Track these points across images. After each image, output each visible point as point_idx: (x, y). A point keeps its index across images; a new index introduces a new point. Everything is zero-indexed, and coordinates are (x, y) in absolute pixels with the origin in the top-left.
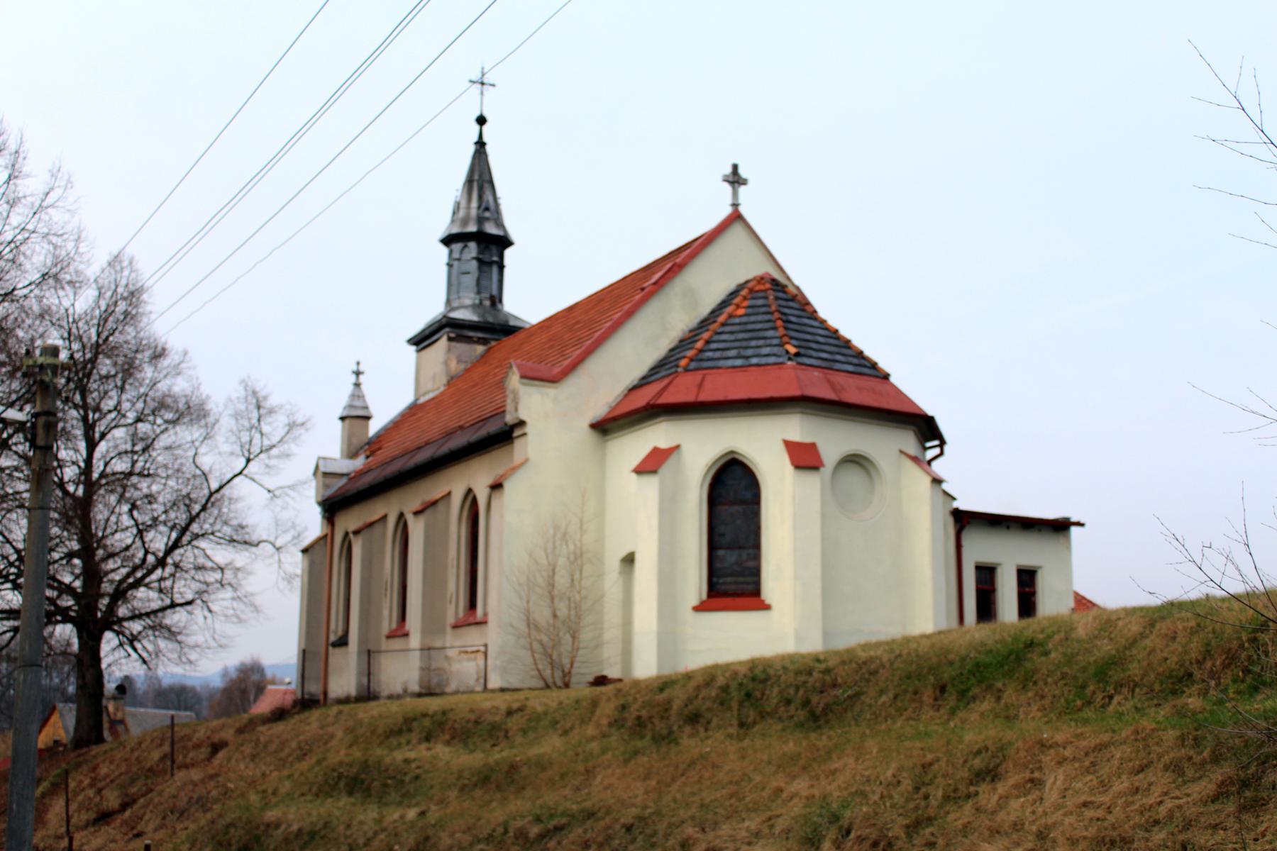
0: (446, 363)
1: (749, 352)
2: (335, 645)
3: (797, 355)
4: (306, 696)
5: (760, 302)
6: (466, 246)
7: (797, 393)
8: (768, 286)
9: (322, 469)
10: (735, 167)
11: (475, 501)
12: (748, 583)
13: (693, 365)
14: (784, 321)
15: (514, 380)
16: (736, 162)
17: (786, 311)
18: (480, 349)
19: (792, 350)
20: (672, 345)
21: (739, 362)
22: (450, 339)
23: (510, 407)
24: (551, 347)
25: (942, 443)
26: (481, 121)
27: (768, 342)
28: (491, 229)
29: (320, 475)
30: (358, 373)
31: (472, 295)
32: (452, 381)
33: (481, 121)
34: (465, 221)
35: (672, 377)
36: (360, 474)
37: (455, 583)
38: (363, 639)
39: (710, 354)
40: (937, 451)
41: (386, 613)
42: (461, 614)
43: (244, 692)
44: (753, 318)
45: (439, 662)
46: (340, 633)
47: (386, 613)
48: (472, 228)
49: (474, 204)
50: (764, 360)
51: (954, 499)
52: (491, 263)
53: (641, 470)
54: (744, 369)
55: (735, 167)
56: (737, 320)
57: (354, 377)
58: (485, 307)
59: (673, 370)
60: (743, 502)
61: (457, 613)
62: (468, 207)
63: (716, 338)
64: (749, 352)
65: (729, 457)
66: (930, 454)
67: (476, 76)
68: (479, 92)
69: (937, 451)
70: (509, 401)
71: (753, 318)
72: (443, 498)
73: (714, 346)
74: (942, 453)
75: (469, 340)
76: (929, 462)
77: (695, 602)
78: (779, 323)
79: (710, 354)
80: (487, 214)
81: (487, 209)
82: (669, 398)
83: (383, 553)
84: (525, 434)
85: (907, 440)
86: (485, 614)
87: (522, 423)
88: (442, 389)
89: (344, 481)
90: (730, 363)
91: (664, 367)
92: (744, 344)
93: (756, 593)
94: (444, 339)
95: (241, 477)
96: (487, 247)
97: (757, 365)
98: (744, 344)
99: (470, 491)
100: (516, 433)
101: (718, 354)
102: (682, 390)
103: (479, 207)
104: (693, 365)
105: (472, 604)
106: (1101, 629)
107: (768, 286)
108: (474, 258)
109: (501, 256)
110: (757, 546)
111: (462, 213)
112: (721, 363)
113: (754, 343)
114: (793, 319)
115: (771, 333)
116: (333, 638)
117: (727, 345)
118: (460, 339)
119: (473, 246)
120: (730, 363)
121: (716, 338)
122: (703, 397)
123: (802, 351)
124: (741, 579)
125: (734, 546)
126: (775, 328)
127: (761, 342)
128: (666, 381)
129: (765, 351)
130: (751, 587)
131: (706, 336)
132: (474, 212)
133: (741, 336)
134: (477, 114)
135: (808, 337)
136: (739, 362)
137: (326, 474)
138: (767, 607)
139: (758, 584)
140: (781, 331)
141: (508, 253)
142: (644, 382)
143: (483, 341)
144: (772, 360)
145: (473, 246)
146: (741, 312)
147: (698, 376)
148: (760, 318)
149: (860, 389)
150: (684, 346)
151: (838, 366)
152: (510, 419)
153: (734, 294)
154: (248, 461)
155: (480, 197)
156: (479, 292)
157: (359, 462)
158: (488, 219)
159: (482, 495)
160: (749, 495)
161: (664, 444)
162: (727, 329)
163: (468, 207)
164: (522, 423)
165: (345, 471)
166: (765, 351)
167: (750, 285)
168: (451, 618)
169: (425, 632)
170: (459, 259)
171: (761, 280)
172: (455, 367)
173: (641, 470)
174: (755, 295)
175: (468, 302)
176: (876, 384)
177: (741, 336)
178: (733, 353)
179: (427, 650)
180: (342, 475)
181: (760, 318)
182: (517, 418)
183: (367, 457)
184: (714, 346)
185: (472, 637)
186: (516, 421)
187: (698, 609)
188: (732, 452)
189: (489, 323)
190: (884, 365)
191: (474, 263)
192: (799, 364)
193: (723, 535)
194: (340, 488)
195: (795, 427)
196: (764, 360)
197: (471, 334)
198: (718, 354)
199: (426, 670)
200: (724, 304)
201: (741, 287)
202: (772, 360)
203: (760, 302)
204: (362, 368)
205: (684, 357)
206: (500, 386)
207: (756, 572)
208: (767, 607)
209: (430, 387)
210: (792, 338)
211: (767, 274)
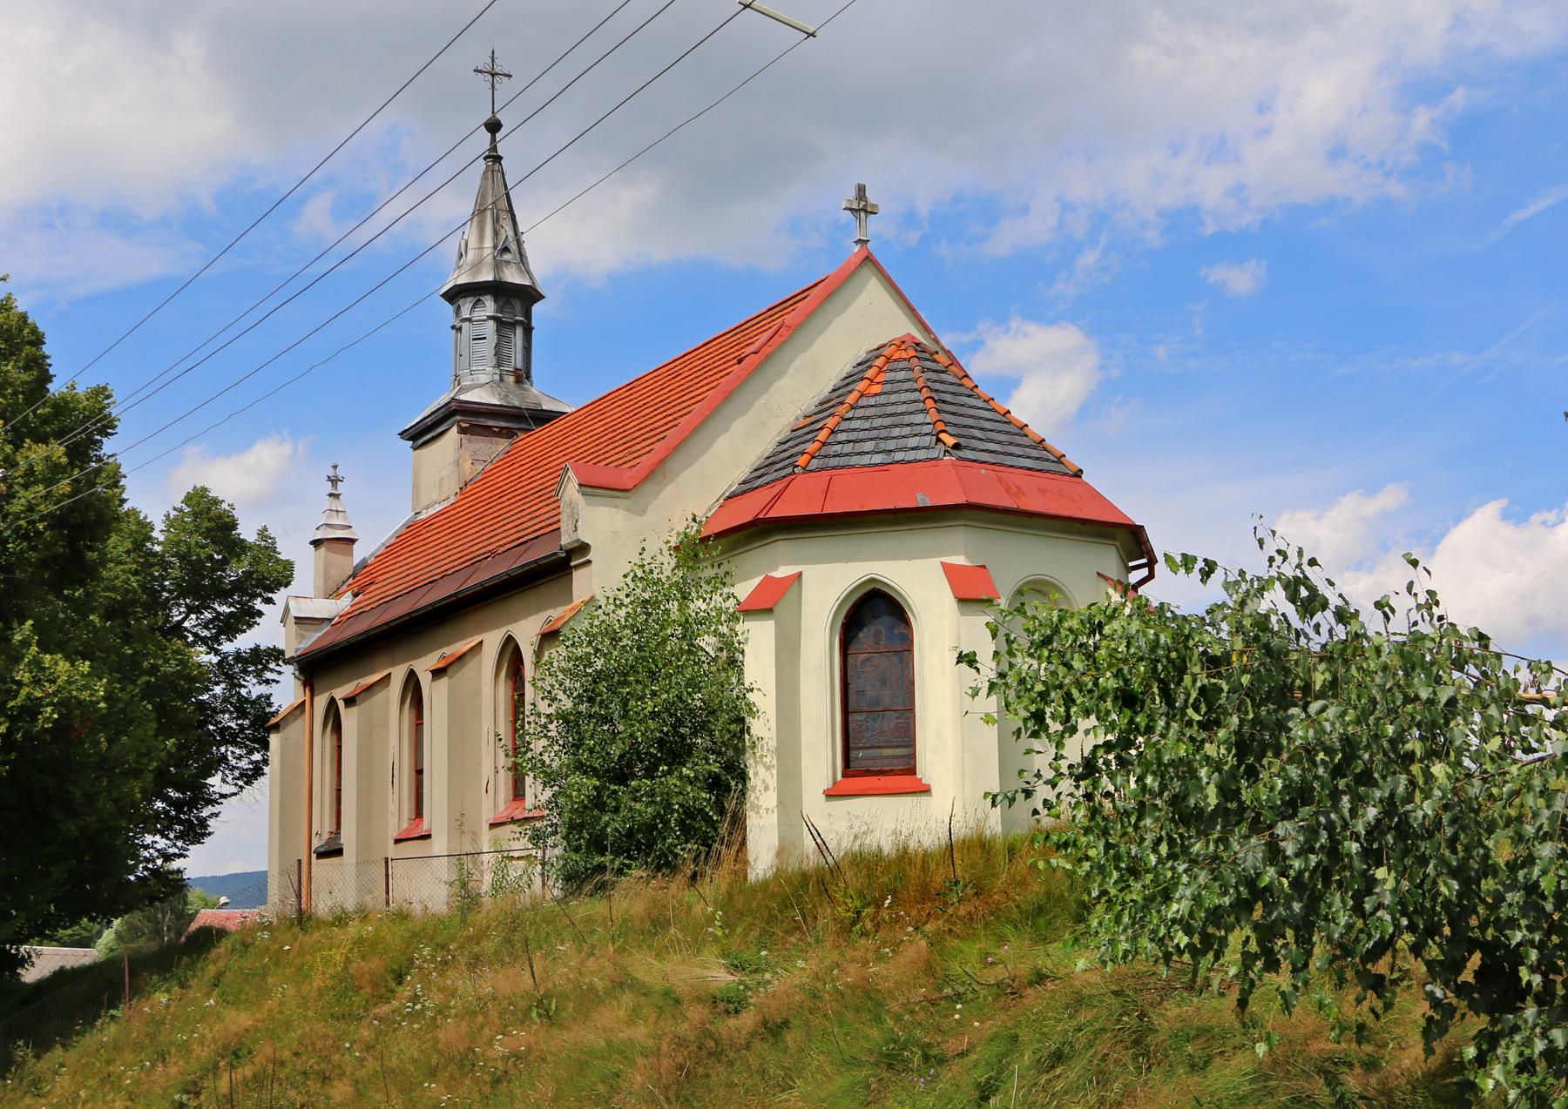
0: (457, 463)
1: (891, 445)
3: (957, 447)
5: (902, 375)
6: (479, 300)
7: (961, 500)
8: (912, 353)
9: (294, 613)
10: (861, 190)
13: (815, 463)
14: (935, 401)
16: (862, 183)
17: (937, 386)
18: (502, 445)
19: (950, 441)
21: (878, 459)
22: (462, 431)
23: (566, 526)
24: (611, 441)
27: (917, 430)
28: (512, 276)
29: (291, 621)
30: (334, 481)
33: (493, 127)
34: (477, 266)
35: (787, 479)
36: (349, 617)
38: (364, 845)
39: (838, 448)
40: (1144, 572)
41: (392, 807)
42: (502, 807)
44: (893, 398)
47: (392, 807)
48: (487, 276)
50: (911, 455)
52: (513, 325)
54: (886, 467)
55: (861, 190)
56: (872, 401)
57: (328, 487)
63: (844, 425)
64: (891, 445)
65: (869, 587)
66: (1134, 577)
67: (483, 62)
69: (1144, 572)
70: (563, 517)
71: (893, 398)
72: (472, 649)
73: (842, 437)
74: (1151, 576)
75: (487, 431)
76: (1135, 587)
77: (826, 783)
78: (930, 403)
79: (838, 448)
80: (507, 257)
81: (506, 250)
82: (781, 510)
83: (386, 725)
84: (589, 562)
85: (1107, 559)
87: (583, 548)
90: (865, 460)
92: (884, 433)
93: (912, 771)
94: (455, 428)
96: (508, 303)
97: (902, 462)
98: (884, 433)
101: (848, 448)
103: (495, 247)
104: (815, 463)
105: (419, 813)
107: (912, 353)
108: (490, 318)
109: (528, 315)
110: (910, 709)
111: (471, 256)
112: (854, 460)
113: (896, 432)
114: (948, 397)
115: (919, 418)
116: (316, 843)
117: (861, 435)
119: (489, 306)
120: (865, 460)
121: (844, 425)
123: (963, 441)
126: (925, 411)
127: (907, 430)
128: (780, 486)
129: (913, 442)
131: (831, 422)
133: (877, 422)
134: (487, 116)
135: (970, 422)
136: (878, 459)
137: (299, 620)
138: (925, 790)
140: (932, 416)
141: (537, 309)
142: (747, 487)
143: (509, 434)
144: (922, 455)
145: (489, 306)
146: (876, 389)
147: (825, 475)
148: (904, 397)
149: (1043, 492)
151: (1009, 461)
152: (566, 540)
153: (864, 364)
155: (496, 233)
156: (499, 365)
157: (345, 603)
162: (860, 413)
164: (583, 548)
166: (913, 442)
167: (886, 352)
170: (469, 320)
171: (901, 344)
174: (895, 365)
175: (484, 379)
176: (1067, 484)
177: (877, 422)
178: (869, 446)
180: (323, 620)
181: (904, 397)
182: (578, 540)
183: (355, 595)
184: (842, 437)
187: (830, 795)
188: (872, 580)
190: (1074, 459)
191: (491, 325)
192: (960, 459)
197: (490, 423)
198: (848, 448)
200: (850, 380)
201: (877, 352)
202: (922, 455)
203: (902, 375)
204: (340, 473)
205: (803, 453)
206: (550, 496)
208: (925, 790)
209: (435, 496)
210: (946, 424)
211: (909, 334)
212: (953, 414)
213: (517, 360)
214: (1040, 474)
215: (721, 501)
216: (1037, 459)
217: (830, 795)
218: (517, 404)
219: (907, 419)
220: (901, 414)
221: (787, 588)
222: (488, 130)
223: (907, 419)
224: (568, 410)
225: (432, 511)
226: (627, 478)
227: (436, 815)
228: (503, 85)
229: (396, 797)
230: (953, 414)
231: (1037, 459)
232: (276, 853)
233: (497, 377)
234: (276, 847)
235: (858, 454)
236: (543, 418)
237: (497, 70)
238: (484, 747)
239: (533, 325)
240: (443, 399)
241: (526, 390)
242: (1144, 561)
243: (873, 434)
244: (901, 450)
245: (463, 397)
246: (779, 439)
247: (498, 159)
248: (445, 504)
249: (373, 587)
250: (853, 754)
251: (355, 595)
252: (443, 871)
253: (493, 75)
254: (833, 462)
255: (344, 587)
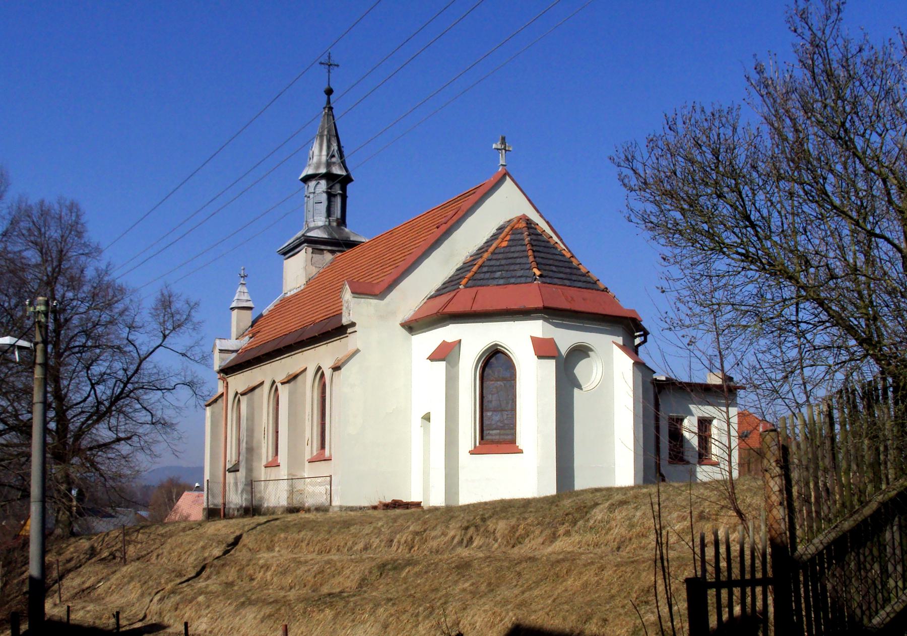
2: (230, 471)
4: (211, 506)
11: (323, 375)
12: (507, 435)
15: (347, 295)
20: (458, 266)
25: (646, 334)
26: (329, 92)
27: (522, 266)
28: (337, 170)
31: (324, 219)
32: (309, 282)
36: (246, 351)
37: (310, 430)
39: (482, 276)
43: (170, 493)
44: (513, 249)
45: (299, 485)
46: (233, 462)
48: (323, 170)
49: (324, 152)
51: (655, 372)
53: (434, 358)
58: (332, 227)
59: (456, 287)
60: (504, 379)
61: (312, 453)
62: (320, 155)
68: (332, 58)
70: (344, 308)
71: (513, 249)
74: (645, 341)
77: (471, 448)
79: (482, 276)
86: (331, 455)
88: (302, 287)
89: (234, 355)
91: (451, 285)
93: (513, 441)
95: (161, 347)
99: (319, 368)
100: (349, 330)
102: (463, 301)
103: (327, 155)
105: (323, 446)
106: (96, 618)
110: (514, 409)
116: (228, 466)
118: (316, 251)
122: (477, 307)
124: (502, 432)
125: (498, 410)
130: (510, 437)
131: (480, 262)
132: (324, 158)
134: (326, 86)
138: (521, 452)
139: (514, 434)
142: (439, 293)
147: (475, 289)
150: (469, 266)
152: (345, 321)
154: (165, 337)
155: (329, 147)
158: (334, 163)
159: (328, 373)
160: (507, 375)
161: (450, 340)
163: (320, 155)
165: (235, 348)
168: (308, 456)
169: (290, 466)
172: (314, 271)
173: (434, 358)
175: (321, 224)
177: (503, 262)
179: (291, 479)
180: (233, 351)
185: (322, 468)
186: (349, 323)
187: (472, 453)
188: (496, 345)
189: (335, 239)
193: (491, 402)
194: (234, 359)
195: (537, 328)
196: (519, 280)
199: (291, 492)
201: (501, 229)
207: (513, 426)
208: (521, 452)
212: (542, 258)
213: (338, 213)
214: (585, 290)
215: (425, 300)
216: (584, 282)
217: (472, 453)
218: (337, 237)
219: (518, 261)
220: (515, 258)
221: (453, 348)
222: (327, 94)
223: (518, 261)
224: (364, 240)
225: (292, 293)
226: (377, 292)
227: (283, 458)
228: (334, 71)
229: (266, 445)
230: (542, 258)
231: (584, 282)
232: (641, 452)
233: (327, 223)
234: (641, 435)
235: (492, 279)
236: (352, 245)
237: (331, 62)
238: (307, 422)
239: (348, 195)
240: (299, 234)
241: (343, 230)
242: (642, 333)
243: (501, 268)
244: (513, 277)
245: (309, 234)
246: (457, 267)
247: (331, 109)
248: (299, 290)
249: (259, 334)
250: (485, 432)
251: (251, 338)
252: (284, 486)
253: (329, 66)
254: (480, 283)
255: (247, 332)
